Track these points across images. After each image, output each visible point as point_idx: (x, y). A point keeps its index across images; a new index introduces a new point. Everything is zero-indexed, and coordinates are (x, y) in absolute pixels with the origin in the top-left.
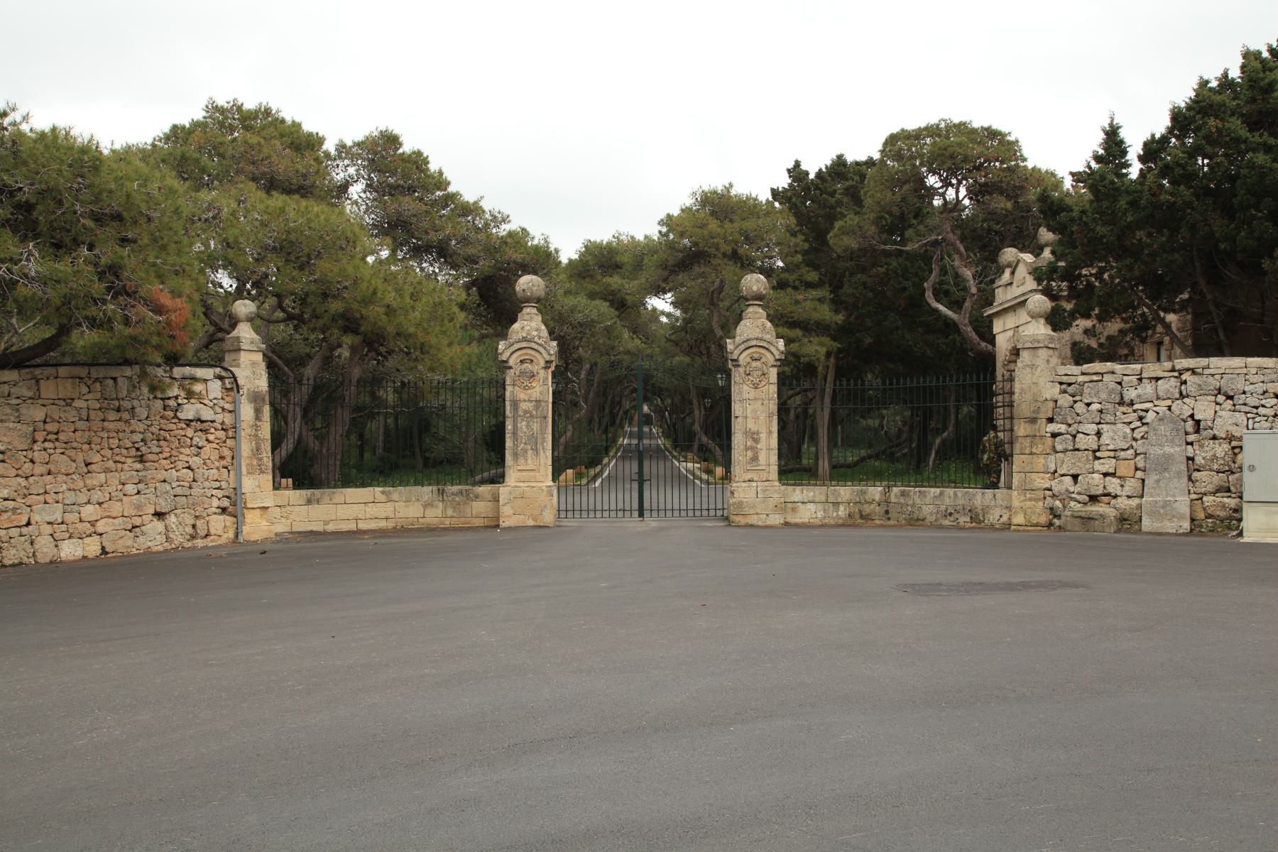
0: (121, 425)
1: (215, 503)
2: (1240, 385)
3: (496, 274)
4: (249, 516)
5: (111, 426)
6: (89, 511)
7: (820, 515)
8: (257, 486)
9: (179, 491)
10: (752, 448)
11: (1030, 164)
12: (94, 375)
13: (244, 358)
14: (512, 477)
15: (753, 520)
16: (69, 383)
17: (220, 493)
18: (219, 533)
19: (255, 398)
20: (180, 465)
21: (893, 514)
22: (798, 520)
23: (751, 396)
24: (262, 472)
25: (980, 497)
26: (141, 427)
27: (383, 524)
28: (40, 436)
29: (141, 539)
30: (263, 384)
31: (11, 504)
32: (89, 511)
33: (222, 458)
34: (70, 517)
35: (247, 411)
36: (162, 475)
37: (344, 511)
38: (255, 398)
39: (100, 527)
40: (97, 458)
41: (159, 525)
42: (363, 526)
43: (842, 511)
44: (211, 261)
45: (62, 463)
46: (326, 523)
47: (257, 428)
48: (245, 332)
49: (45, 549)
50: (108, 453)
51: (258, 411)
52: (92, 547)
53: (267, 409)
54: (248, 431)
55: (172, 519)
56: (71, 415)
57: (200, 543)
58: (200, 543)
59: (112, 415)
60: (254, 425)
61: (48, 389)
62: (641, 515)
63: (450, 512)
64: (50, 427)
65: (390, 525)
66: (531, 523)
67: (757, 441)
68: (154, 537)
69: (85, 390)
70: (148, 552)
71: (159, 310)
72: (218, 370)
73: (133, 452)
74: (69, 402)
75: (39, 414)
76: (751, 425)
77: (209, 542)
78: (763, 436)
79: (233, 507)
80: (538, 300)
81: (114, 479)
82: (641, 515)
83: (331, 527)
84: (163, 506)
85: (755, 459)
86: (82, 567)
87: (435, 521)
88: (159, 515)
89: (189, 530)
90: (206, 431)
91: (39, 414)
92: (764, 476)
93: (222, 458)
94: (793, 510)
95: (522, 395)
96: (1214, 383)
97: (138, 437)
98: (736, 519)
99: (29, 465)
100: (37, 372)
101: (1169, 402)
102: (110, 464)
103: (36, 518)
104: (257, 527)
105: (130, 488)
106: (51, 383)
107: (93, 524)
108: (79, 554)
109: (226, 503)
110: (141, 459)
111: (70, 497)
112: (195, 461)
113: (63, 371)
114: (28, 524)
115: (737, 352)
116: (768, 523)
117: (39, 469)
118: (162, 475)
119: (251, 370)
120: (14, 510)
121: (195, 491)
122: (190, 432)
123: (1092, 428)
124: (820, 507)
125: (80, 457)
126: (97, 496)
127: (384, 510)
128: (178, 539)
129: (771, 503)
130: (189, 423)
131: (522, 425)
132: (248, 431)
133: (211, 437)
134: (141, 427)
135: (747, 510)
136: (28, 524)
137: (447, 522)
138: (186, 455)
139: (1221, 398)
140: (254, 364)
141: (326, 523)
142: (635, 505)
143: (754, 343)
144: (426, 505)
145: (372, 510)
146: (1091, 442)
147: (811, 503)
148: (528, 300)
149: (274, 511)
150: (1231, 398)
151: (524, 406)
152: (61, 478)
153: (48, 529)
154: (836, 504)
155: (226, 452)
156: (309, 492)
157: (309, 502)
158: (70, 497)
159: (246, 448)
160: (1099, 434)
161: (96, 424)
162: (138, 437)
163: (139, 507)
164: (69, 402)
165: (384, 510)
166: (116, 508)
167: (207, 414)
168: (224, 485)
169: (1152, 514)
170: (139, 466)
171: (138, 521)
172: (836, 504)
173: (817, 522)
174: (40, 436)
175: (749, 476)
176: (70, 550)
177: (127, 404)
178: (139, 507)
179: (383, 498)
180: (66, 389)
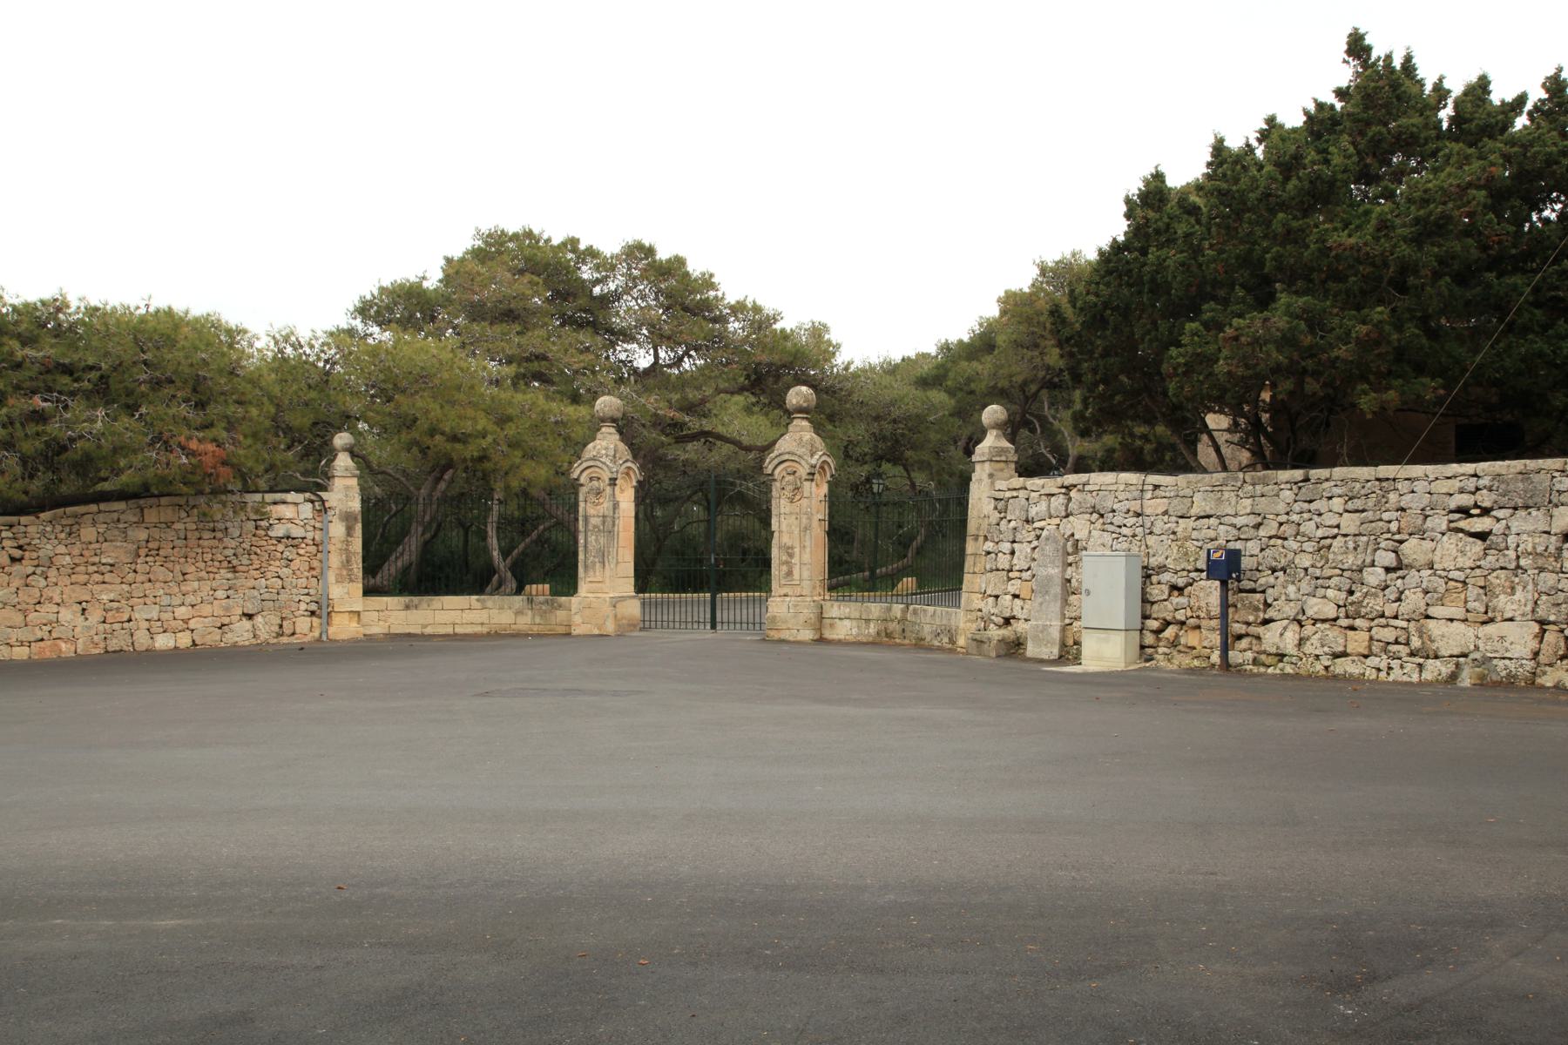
0: (212, 542)
1: (303, 606)
2: (1109, 504)
3: (775, 367)
4: (336, 619)
5: (206, 543)
6: (182, 612)
7: (854, 631)
8: (346, 593)
9: (266, 596)
10: (787, 563)
11: (1092, 256)
12: (192, 503)
13: (338, 483)
14: (583, 588)
15: (785, 635)
16: (169, 511)
17: (308, 599)
18: (306, 631)
19: (348, 518)
20: (269, 575)
21: (908, 634)
22: (835, 637)
23: (787, 510)
24: (351, 581)
25: (930, 617)
26: (233, 544)
27: (478, 629)
28: (143, 552)
29: (229, 635)
30: (356, 505)
31: (115, 605)
32: (182, 612)
33: (312, 569)
34: (164, 616)
35: (337, 529)
36: (252, 583)
37: (442, 617)
38: (348, 518)
39: (192, 624)
40: (193, 569)
41: (246, 624)
42: (459, 630)
43: (872, 629)
44: (1512, 208)
45: (160, 572)
46: (425, 626)
47: (348, 543)
48: (343, 461)
49: (142, 641)
50: (202, 565)
51: (349, 531)
52: (184, 640)
53: (359, 527)
54: (339, 546)
55: (259, 619)
56: (171, 535)
57: (284, 640)
58: (284, 640)
59: (207, 535)
60: (343, 541)
61: (151, 516)
62: (713, 626)
63: (538, 620)
64: (151, 545)
65: (485, 630)
66: (596, 632)
67: (791, 556)
68: (241, 633)
69: (183, 514)
70: (235, 645)
71: (191, 454)
72: (308, 495)
73: (225, 564)
74: (169, 525)
75: (143, 535)
76: (786, 540)
77: (293, 640)
78: (797, 550)
79: (321, 610)
80: (614, 420)
81: (206, 587)
82: (713, 626)
83: (429, 631)
84: (250, 609)
85: (790, 573)
86: (174, 656)
87: (525, 628)
88: (250, 617)
89: (276, 629)
90: (296, 546)
91: (143, 535)
92: (798, 591)
93: (312, 569)
94: (831, 625)
95: (591, 511)
96: (1090, 500)
97: (229, 552)
98: (772, 633)
99: (132, 575)
100: (142, 502)
101: (1057, 521)
102: (203, 574)
103: (136, 615)
104: (343, 628)
105: (221, 594)
106: (154, 511)
107: (186, 621)
108: (171, 644)
109: (314, 607)
110: (234, 570)
111: (165, 600)
112: (285, 572)
113: (164, 500)
114: (130, 620)
115: (771, 467)
116: (799, 638)
117: (140, 578)
118: (252, 583)
119: (345, 492)
120: (118, 609)
121: (283, 597)
122: (280, 547)
123: (1006, 547)
124: (855, 623)
125: (178, 567)
126: (190, 599)
127: (482, 616)
128: (264, 635)
129: (802, 618)
130: (279, 540)
131: (592, 539)
132: (339, 546)
133: (302, 552)
134: (233, 544)
135: (780, 625)
136: (130, 620)
137: (535, 628)
138: (275, 567)
139: (1095, 516)
140: (347, 488)
141: (425, 626)
142: (708, 616)
143: (786, 457)
144: (519, 613)
145: (469, 616)
146: (1003, 561)
147: (851, 619)
148: (603, 420)
149: (358, 613)
150: (1102, 516)
151: (594, 521)
152: (158, 585)
153: (146, 625)
154: (868, 621)
155: (315, 564)
156: (407, 599)
157: (407, 607)
158: (165, 600)
159: (335, 560)
160: (1013, 553)
161: (192, 542)
162: (229, 552)
163: (227, 609)
164: (169, 525)
165: (482, 616)
166: (206, 609)
167: (297, 532)
168: (312, 592)
169: (1036, 638)
170: (230, 575)
171: (226, 620)
172: (868, 621)
173: (851, 638)
174: (143, 552)
175: (783, 591)
176: (163, 642)
177: (220, 526)
178: (227, 609)
179: (478, 605)
180: (168, 514)
